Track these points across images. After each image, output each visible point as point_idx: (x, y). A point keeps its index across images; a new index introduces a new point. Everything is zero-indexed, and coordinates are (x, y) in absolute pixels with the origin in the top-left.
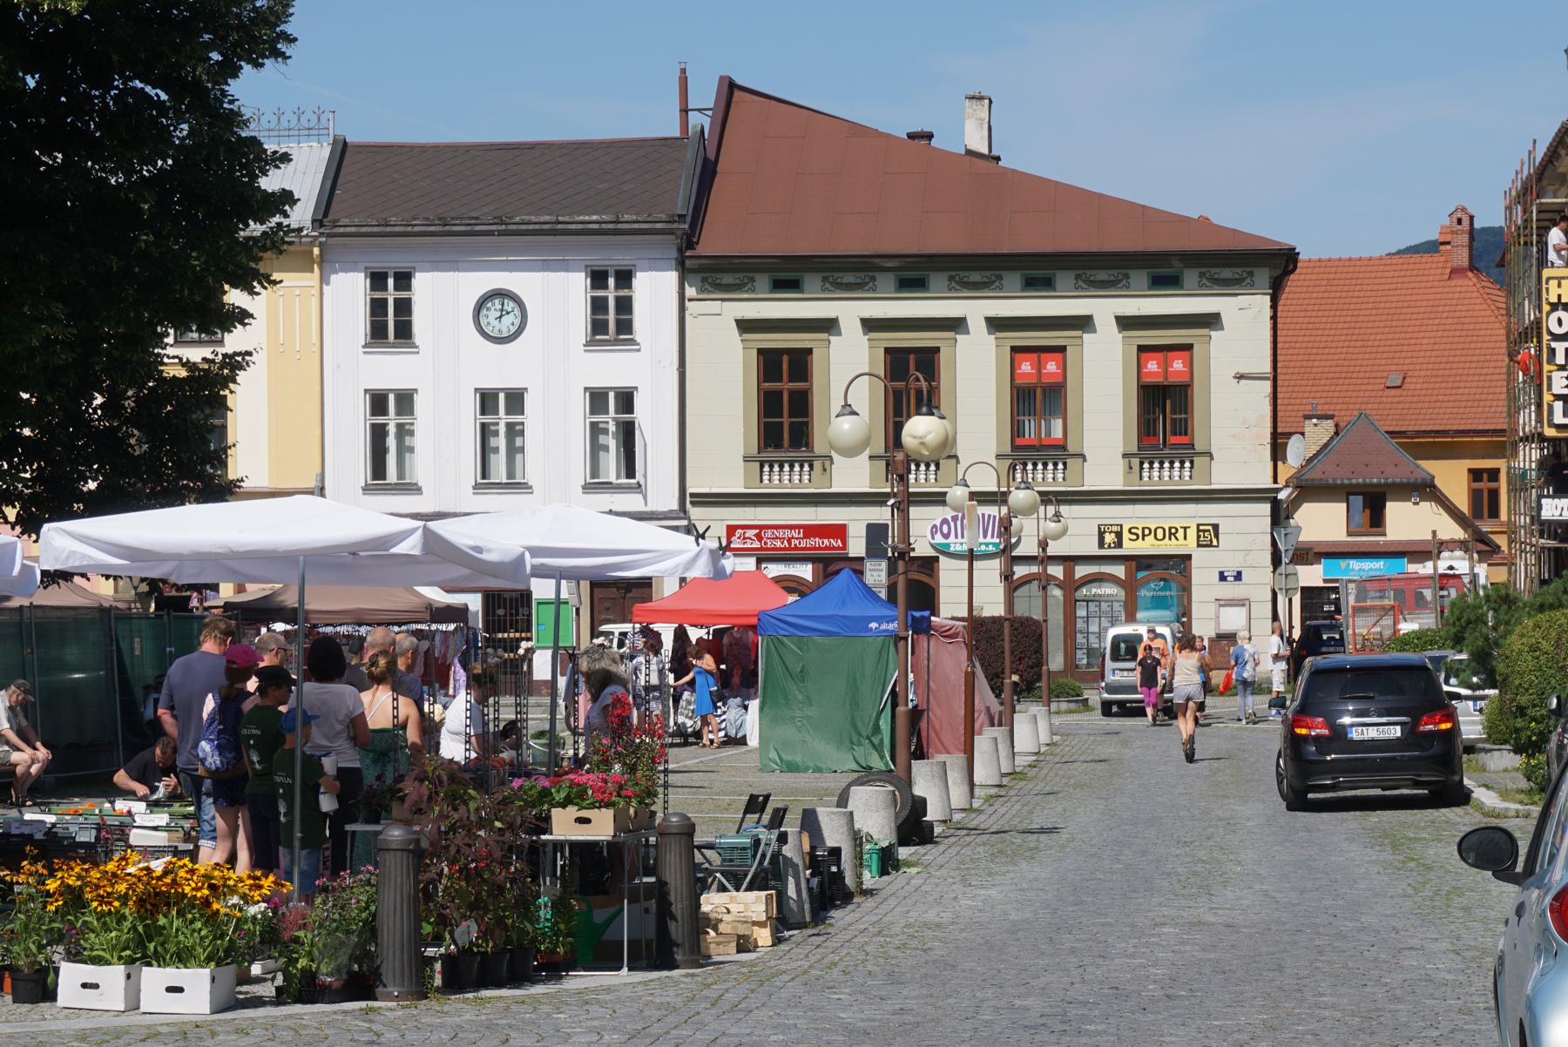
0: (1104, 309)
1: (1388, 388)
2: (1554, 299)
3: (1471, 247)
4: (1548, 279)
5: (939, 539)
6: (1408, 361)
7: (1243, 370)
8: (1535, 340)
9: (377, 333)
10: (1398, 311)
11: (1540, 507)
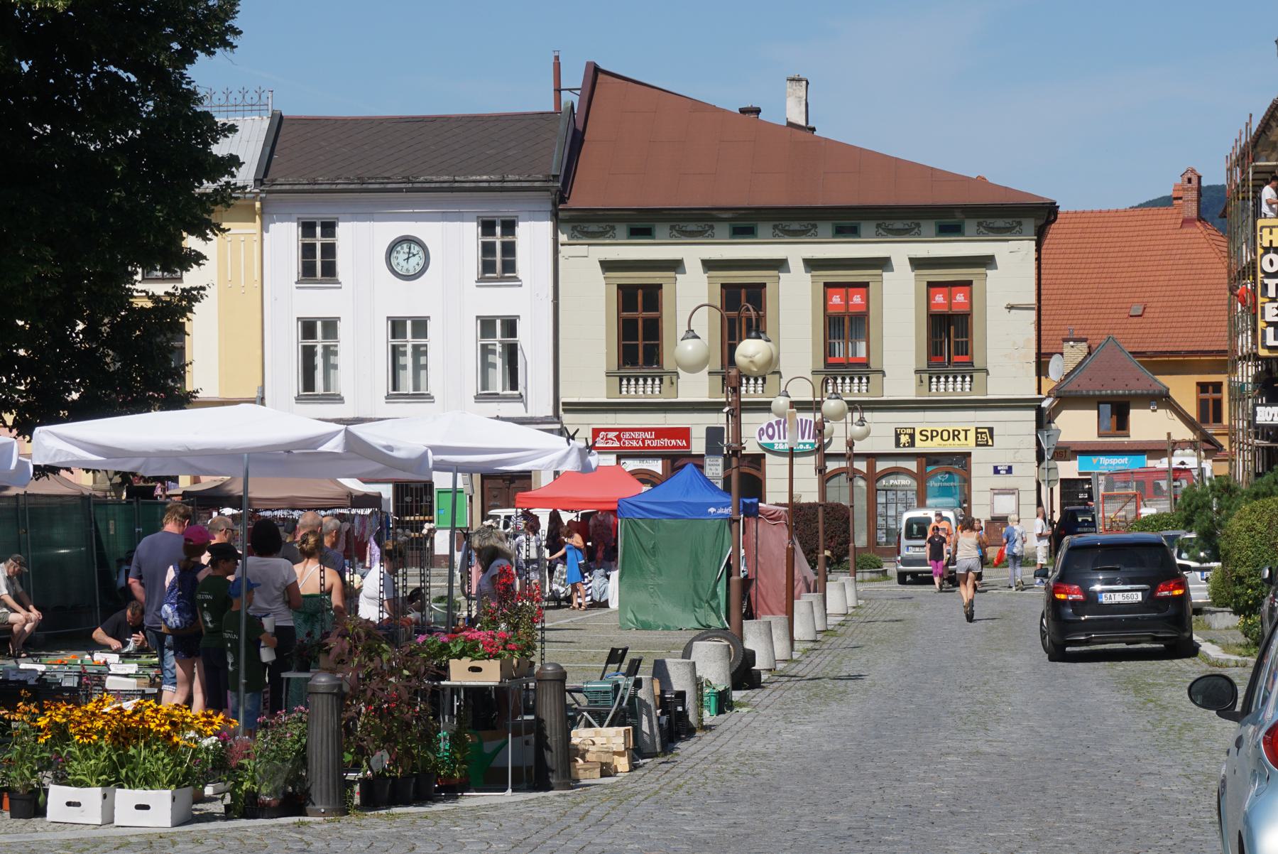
0: (900, 252)
1: (1131, 316)
2: (1266, 244)
3: (1199, 201)
4: (1262, 228)
5: (765, 440)
6: (1147, 294)
7: (1013, 302)
8: (1251, 277)
9: (308, 272)
10: (1140, 253)
11: (1255, 414)
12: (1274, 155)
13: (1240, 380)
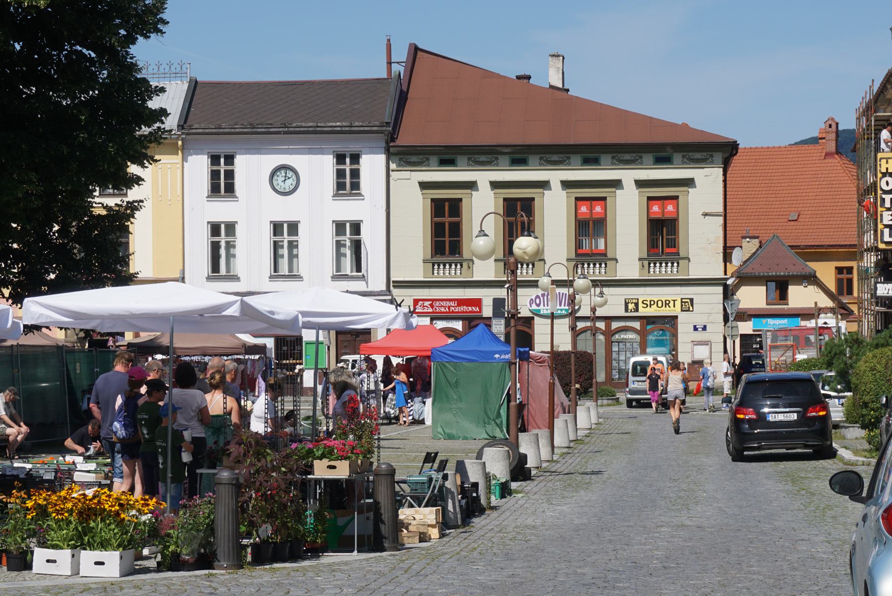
0: (628, 176)
1: (790, 221)
2: (884, 170)
3: (837, 141)
4: (881, 159)
5: (534, 307)
6: (801, 205)
7: (707, 211)
8: (873, 193)
9: (215, 190)
10: (796, 177)
11: (876, 289)
13: (866, 265)
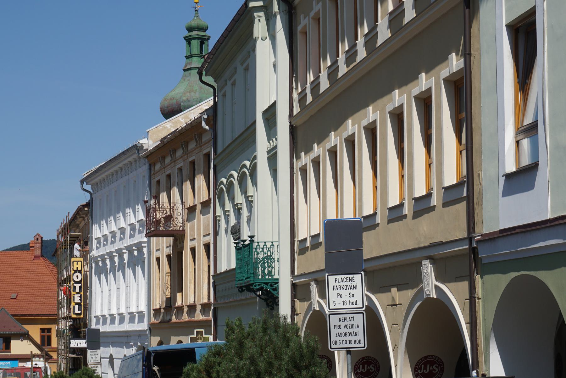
1: (11, 299)
2: (75, 269)
3: (41, 248)
4: (73, 262)
6: (19, 289)
8: (68, 283)
10: (15, 271)
11: (70, 343)
12: (78, 230)
